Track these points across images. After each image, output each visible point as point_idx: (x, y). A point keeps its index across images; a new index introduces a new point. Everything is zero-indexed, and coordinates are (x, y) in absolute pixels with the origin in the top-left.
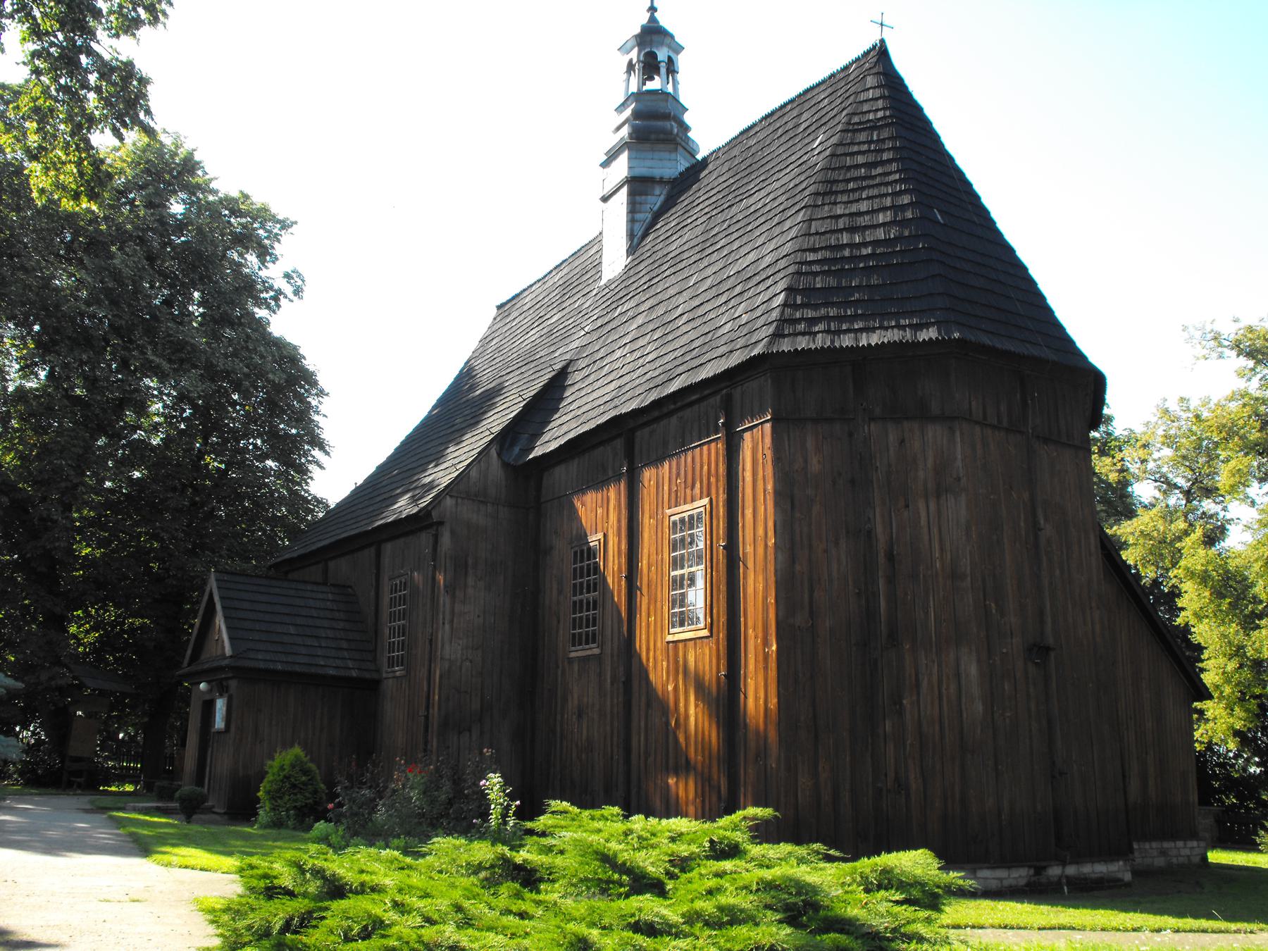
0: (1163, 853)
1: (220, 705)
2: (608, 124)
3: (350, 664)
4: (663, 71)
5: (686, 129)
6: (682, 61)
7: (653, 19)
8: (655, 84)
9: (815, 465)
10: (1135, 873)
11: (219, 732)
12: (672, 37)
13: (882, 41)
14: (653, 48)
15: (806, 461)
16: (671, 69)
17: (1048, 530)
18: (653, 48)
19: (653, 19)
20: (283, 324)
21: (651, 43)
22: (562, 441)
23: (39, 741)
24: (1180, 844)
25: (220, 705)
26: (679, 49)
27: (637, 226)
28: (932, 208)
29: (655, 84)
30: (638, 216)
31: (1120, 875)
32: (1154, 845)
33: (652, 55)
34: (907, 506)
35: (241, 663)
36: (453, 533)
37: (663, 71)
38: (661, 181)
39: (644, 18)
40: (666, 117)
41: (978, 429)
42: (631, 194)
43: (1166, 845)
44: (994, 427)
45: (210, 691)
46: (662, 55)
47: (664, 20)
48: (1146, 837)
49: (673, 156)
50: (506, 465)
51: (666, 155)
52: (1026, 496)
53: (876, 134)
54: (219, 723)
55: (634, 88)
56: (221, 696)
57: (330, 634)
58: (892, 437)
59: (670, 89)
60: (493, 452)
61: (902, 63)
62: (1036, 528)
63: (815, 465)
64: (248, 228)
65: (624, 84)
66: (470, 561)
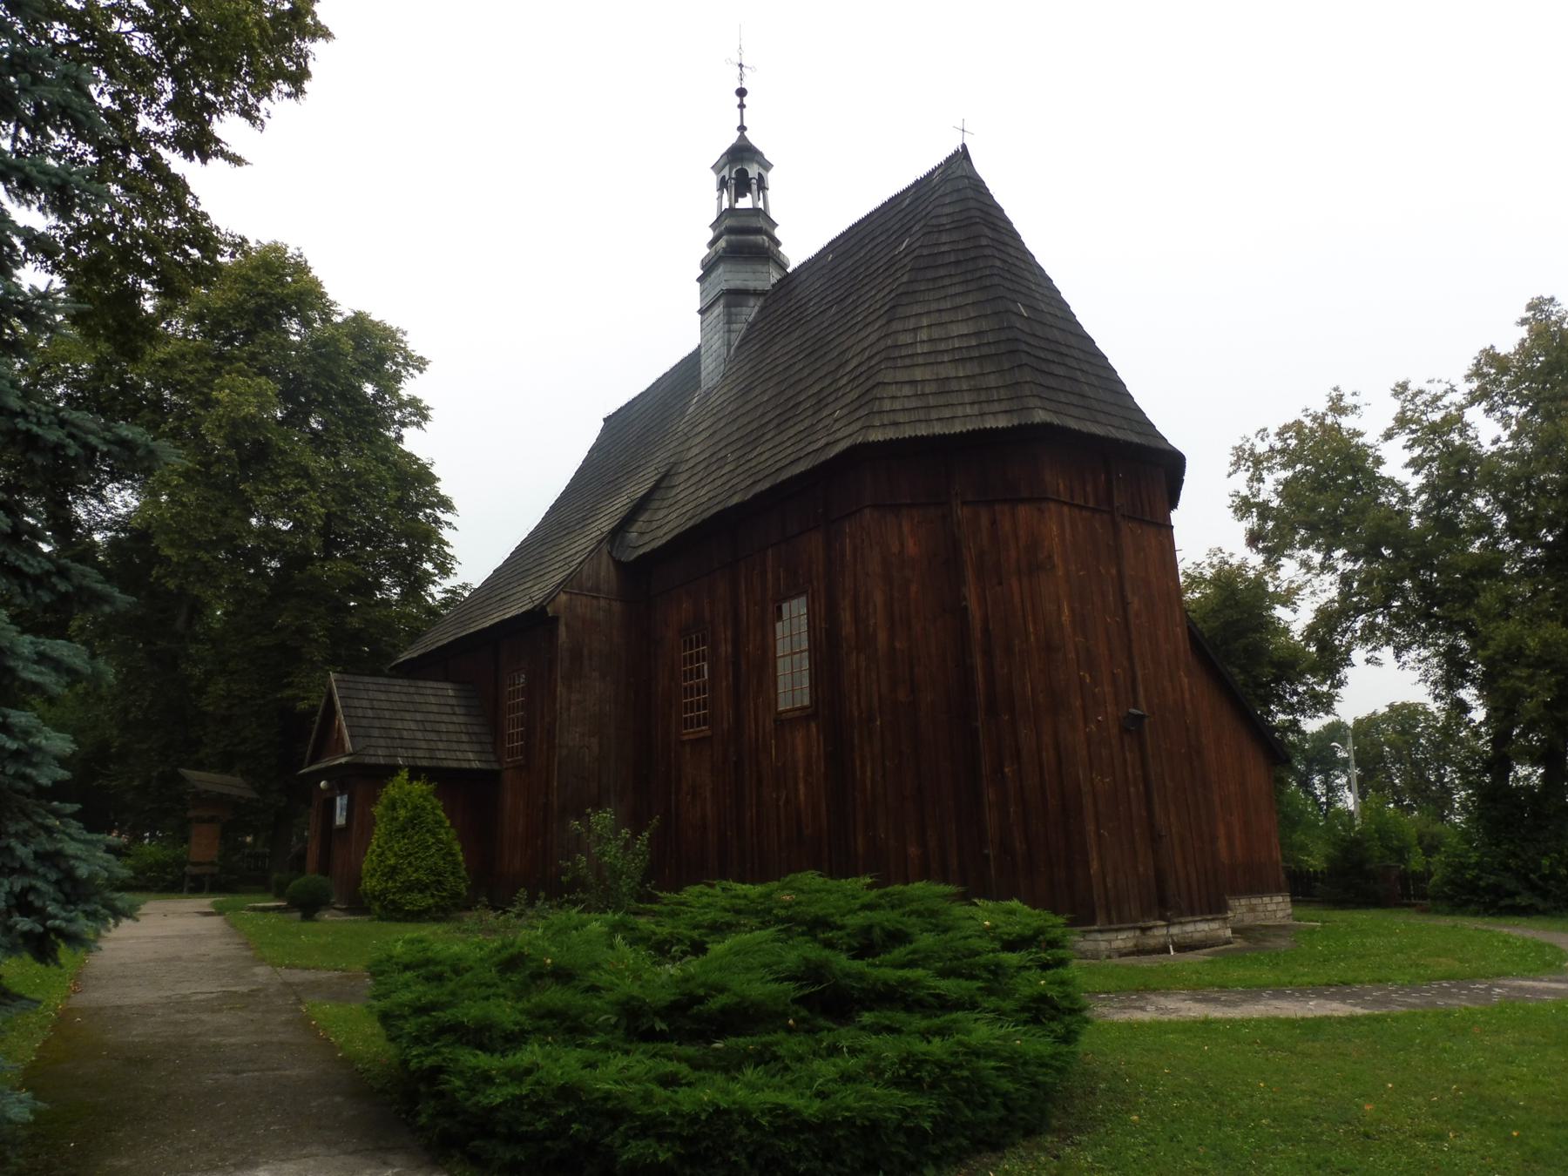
0: (1252, 909)
1: (341, 802)
2: (697, 241)
3: (471, 756)
4: (754, 187)
5: (778, 243)
6: (772, 178)
7: (742, 138)
8: (745, 203)
9: (911, 547)
10: (1234, 931)
11: (341, 829)
12: (761, 154)
13: (964, 146)
14: (742, 167)
15: (902, 545)
16: (762, 186)
17: (1135, 603)
18: (742, 167)
19: (742, 138)
20: (414, 442)
21: (742, 160)
22: (669, 537)
23: (581, 815)
24: (1266, 900)
25: (341, 802)
26: (767, 166)
27: (733, 336)
28: (1015, 302)
29: (745, 203)
30: (734, 327)
31: (1221, 932)
32: (1243, 902)
33: (743, 174)
34: (1000, 583)
35: (359, 760)
36: (567, 625)
37: (754, 187)
38: (756, 293)
39: (732, 138)
40: (759, 231)
41: (1066, 509)
42: (727, 306)
43: (1254, 901)
44: (1081, 507)
45: (330, 789)
46: (753, 171)
47: (753, 137)
48: (1238, 893)
49: (765, 269)
50: (618, 564)
51: (759, 268)
52: (1114, 571)
53: (947, 235)
54: (340, 819)
55: (726, 205)
56: (342, 794)
57: (451, 728)
58: (985, 521)
59: (761, 205)
60: (605, 548)
61: (983, 166)
62: (1124, 604)
63: (911, 547)
64: (373, 349)
65: (716, 202)
66: (586, 652)
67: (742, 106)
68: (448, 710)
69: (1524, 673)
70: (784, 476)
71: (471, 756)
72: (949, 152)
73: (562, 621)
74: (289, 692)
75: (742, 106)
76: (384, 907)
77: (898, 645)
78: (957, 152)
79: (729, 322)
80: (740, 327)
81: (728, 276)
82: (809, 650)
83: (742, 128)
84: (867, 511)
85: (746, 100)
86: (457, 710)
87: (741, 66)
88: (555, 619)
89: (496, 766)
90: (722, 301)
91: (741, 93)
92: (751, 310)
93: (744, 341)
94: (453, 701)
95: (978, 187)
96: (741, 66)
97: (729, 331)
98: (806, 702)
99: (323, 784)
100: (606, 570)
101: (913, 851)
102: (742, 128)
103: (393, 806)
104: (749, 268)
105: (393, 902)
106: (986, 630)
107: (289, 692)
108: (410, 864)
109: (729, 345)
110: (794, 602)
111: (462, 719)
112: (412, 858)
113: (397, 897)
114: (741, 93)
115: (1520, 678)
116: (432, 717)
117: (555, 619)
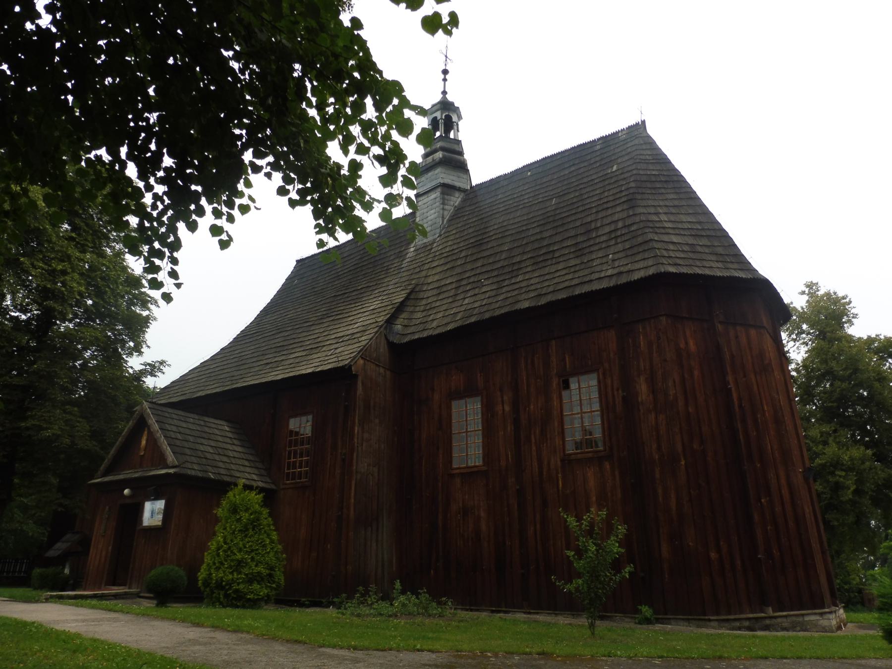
3: (255, 477)
9: (692, 346)
27: (446, 213)
30: (446, 207)
36: (363, 383)
38: (459, 189)
39: (438, 98)
42: (443, 193)
46: (455, 118)
47: (450, 98)
63: (692, 346)
67: (445, 80)
68: (229, 441)
69: (843, 474)
70: (577, 292)
71: (255, 477)
72: (632, 122)
73: (360, 379)
74: (30, 423)
75: (445, 80)
76: (226, 596)
77: (690, 410)
78: (637, 124)
79: (443, 204)
80: (450, 209)
81: (442, 175)
82: (602, 410)
83: (444, 93)
84: (663, 319)
85: (447, 77)
86: (236, 442)
87: (446, 57)
88: (356, 376)
89: (273, 487)
90: (439, 190)
91: (445, 72)
92: (456, 199)
93: (454, 217)
94: (230, 435)
95: (650, 143)
96: (446, 57)
97: (443, 209)
98: (479, 462)
99: (126, 492)
100: (383, 348)
101: (713, 555)
102: (444, 93)
103: (234, 510)
104: (455, 174)
105: (237, 591)
106: (740, 406)
107: (30, 423)
108: (253, 559)
109: (443, 218)
110: (583, 378)
111: (240, 449)
112: (253, 554)
113: (241, 586)
114: (445, 72)
115: (840, 476)
116: (220, 445)
117: (356, 376)
